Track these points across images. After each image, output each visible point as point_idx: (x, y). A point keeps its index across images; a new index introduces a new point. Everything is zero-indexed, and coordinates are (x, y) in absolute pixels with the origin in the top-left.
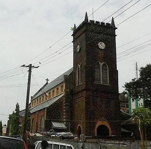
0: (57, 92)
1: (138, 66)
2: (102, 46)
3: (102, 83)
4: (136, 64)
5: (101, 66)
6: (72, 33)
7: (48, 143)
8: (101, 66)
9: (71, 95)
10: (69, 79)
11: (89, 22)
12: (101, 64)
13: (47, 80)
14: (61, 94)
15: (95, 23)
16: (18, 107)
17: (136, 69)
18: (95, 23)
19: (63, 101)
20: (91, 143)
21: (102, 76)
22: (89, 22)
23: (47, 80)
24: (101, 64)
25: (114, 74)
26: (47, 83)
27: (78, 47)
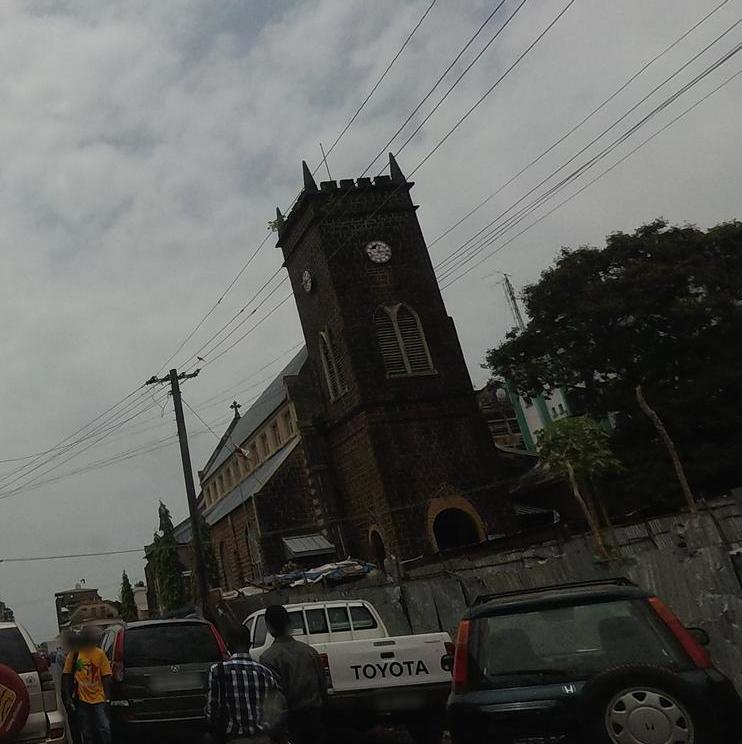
2: (379, 252)
3: (409, 372)
4: (507, 281)
5: (394, 318)
6: (275, 237)
8: (394, 318)
11: (319, 188)
12: (393, 311)
13: (235, 406)
14: (288, 442)
17: (510, 297)
19: (301, 463)
21: (405, 351)
22: (319, 188)
23: (235, 406)
24: (393, 311)
25: (442, 332)
26: (237, 417)
27: (306, 276)
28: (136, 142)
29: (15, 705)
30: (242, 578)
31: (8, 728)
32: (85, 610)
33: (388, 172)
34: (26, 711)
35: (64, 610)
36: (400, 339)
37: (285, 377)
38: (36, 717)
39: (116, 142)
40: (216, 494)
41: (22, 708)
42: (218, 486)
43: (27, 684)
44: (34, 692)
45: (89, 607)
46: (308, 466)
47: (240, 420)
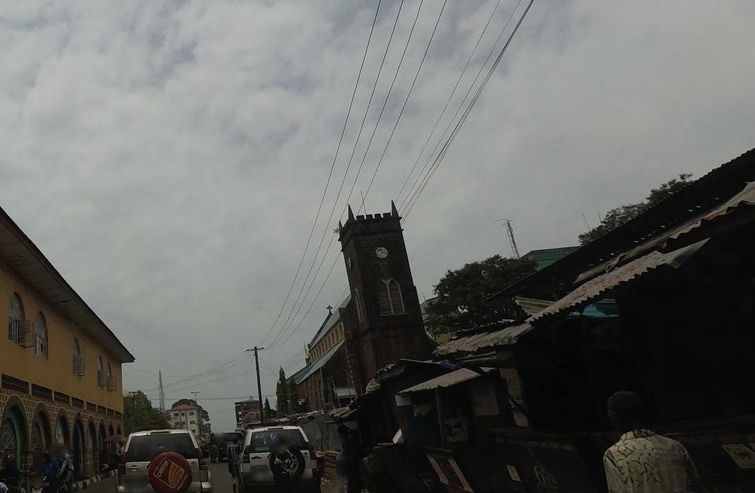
0: (338, 339)
1: (512, 228)
2: (382, 253)
3: (393, 312)
4: (509, 225)
5: (388, 287)
6: (338, 236)
7: (249, 444)
8: (388, 287)
9: (354, 341)
10: (347, 313)
11: (355, 219)
12: (387, 282)
13: (329, 308)
14: (338, 343)
15: (374, 217)
16: (282, 373)
17: (510, 234)
18: (374, 217)
19: (345, 352)
20: (84, 456)
21: (391, 302)
22: (355, 219)
23: (329, 308)
24: (387, 282)
25: (410, 291)
26: (330, 314)
27: (349, 261)
28: (302, 85)
29: (184, 476)
30: (318, 407)
31: (178, 489)
32: (252, 414)
33: (389, 210)
34: (190, 480)
35: (240, 413)
36: (390, 297)
37: (339, 309)
38: (195, 484)
39: (286, 86)
40: (321, 353)
41: (187, 479)
42: (325, 346)
43: (191, 465)
44: (195, 470)
45: (254, 413)
46: (348, 354)
47: (332, 316)
